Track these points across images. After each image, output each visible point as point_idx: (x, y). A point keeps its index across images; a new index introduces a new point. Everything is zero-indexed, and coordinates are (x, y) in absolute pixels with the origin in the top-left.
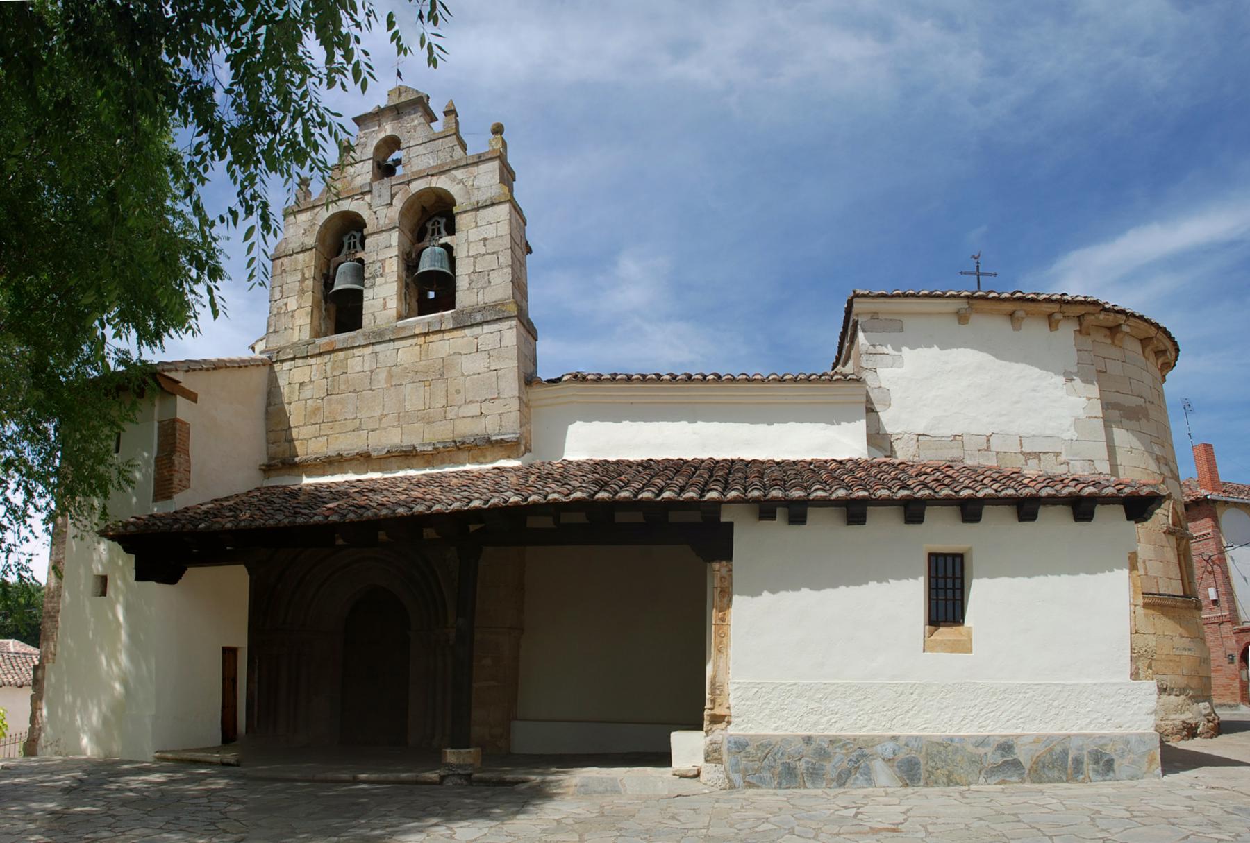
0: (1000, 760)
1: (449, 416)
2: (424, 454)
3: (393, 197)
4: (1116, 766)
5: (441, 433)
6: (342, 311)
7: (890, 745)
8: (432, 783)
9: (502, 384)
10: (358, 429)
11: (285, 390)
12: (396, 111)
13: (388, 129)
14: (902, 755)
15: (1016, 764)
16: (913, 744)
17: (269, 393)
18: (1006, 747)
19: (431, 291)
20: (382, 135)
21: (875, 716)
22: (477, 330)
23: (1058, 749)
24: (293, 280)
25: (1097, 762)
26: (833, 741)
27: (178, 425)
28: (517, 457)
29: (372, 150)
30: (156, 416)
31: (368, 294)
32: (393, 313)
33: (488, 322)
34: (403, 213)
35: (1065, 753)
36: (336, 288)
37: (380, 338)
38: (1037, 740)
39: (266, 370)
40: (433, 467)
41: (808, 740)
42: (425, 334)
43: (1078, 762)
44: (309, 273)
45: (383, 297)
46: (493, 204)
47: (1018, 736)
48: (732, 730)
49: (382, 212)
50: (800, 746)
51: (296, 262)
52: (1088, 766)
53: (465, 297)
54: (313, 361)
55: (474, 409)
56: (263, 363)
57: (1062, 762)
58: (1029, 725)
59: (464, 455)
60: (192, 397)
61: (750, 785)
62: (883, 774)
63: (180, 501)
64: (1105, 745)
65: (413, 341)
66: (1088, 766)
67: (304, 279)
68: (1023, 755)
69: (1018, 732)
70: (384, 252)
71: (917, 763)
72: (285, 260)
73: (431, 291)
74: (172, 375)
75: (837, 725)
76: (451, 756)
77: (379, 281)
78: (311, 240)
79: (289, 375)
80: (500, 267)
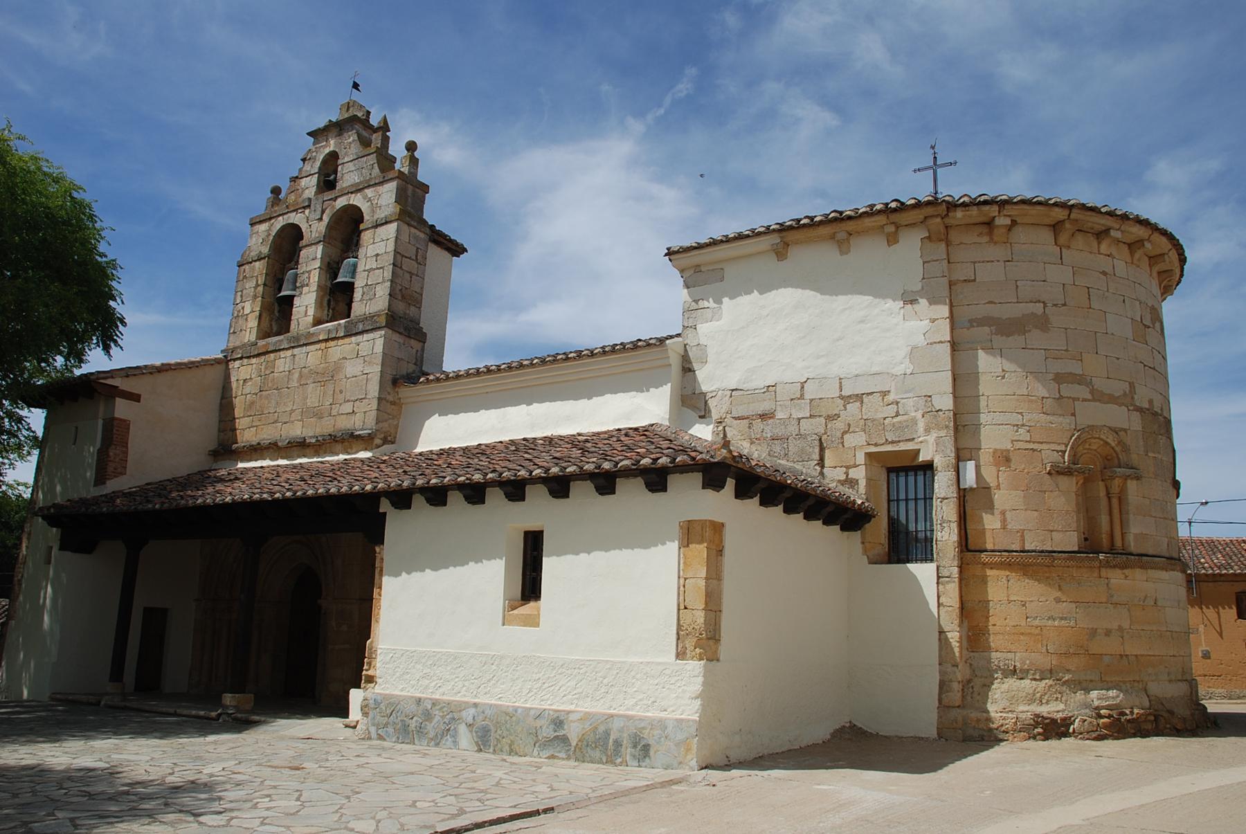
0: (553, 734)
1: (334, 412)
2: (309, 445)
3: (323, 212)
4: (652, 752)
5: (325, 427)
6: (278, 312)
7: (472, 711)
8: (212, 719)
9: (369, 386)
10: (276, 422)
11: (234, 385)
12: (337, 128)
13: (331, 145)
14: (479, 723)
15: (564, 740)
16: (488, 712)
17: (224, 387)
18: (558, 723)
19: (338, 296)
20: (327, 151)
21: (466, 684)
22: (359, 338)
23: (602, 729)
24: (250, 284)
25: (635, 747)
26: (435, 703)
27: (115, 423)
28: (370, 450)
29: (318, 164)
30: (101, 414)
31: (297, 301)
32: (310, 319)
33: (367, 331)
34: (330, 227)
35: (607, 733)
36: (282, 294)
37: (297, 343)
38: (587, 716)
39: (223, 367)
40: (319, 456)
41: (419, 701)
42: (326, 340)
43: (618, 744)
44: (261, 281)
45: (306, 304)
46: (386, 223)
47: (569, 712)
48: (378, 689)
49: (315, 225)
50: (413, 707)
51: (253, 269)
52: (628, 751)
53: (358, 309)
54: (254, 361)
55: (348, 408)
56: (217, 361)
57: (604, 743)
58: (580, 702)
59: (339, 447)
60: (136, 398)
61: (380, 738)
62: (465, 738)
63: (112, 486)
64: (644, 728)
65: (317, 346)
66: (628, 751)
67: (257, 285)
68: (573, 732)
69: (572, 707)
70: (311, 261)
71: (489, 731)
72: (247, 267)
73: (338, 296)
74: (109, 382)
75: (441, 690)
76: (228, 699)
77: (305, 289)
78: (265, 250)
79: (241, 372)
80: (384, 281)
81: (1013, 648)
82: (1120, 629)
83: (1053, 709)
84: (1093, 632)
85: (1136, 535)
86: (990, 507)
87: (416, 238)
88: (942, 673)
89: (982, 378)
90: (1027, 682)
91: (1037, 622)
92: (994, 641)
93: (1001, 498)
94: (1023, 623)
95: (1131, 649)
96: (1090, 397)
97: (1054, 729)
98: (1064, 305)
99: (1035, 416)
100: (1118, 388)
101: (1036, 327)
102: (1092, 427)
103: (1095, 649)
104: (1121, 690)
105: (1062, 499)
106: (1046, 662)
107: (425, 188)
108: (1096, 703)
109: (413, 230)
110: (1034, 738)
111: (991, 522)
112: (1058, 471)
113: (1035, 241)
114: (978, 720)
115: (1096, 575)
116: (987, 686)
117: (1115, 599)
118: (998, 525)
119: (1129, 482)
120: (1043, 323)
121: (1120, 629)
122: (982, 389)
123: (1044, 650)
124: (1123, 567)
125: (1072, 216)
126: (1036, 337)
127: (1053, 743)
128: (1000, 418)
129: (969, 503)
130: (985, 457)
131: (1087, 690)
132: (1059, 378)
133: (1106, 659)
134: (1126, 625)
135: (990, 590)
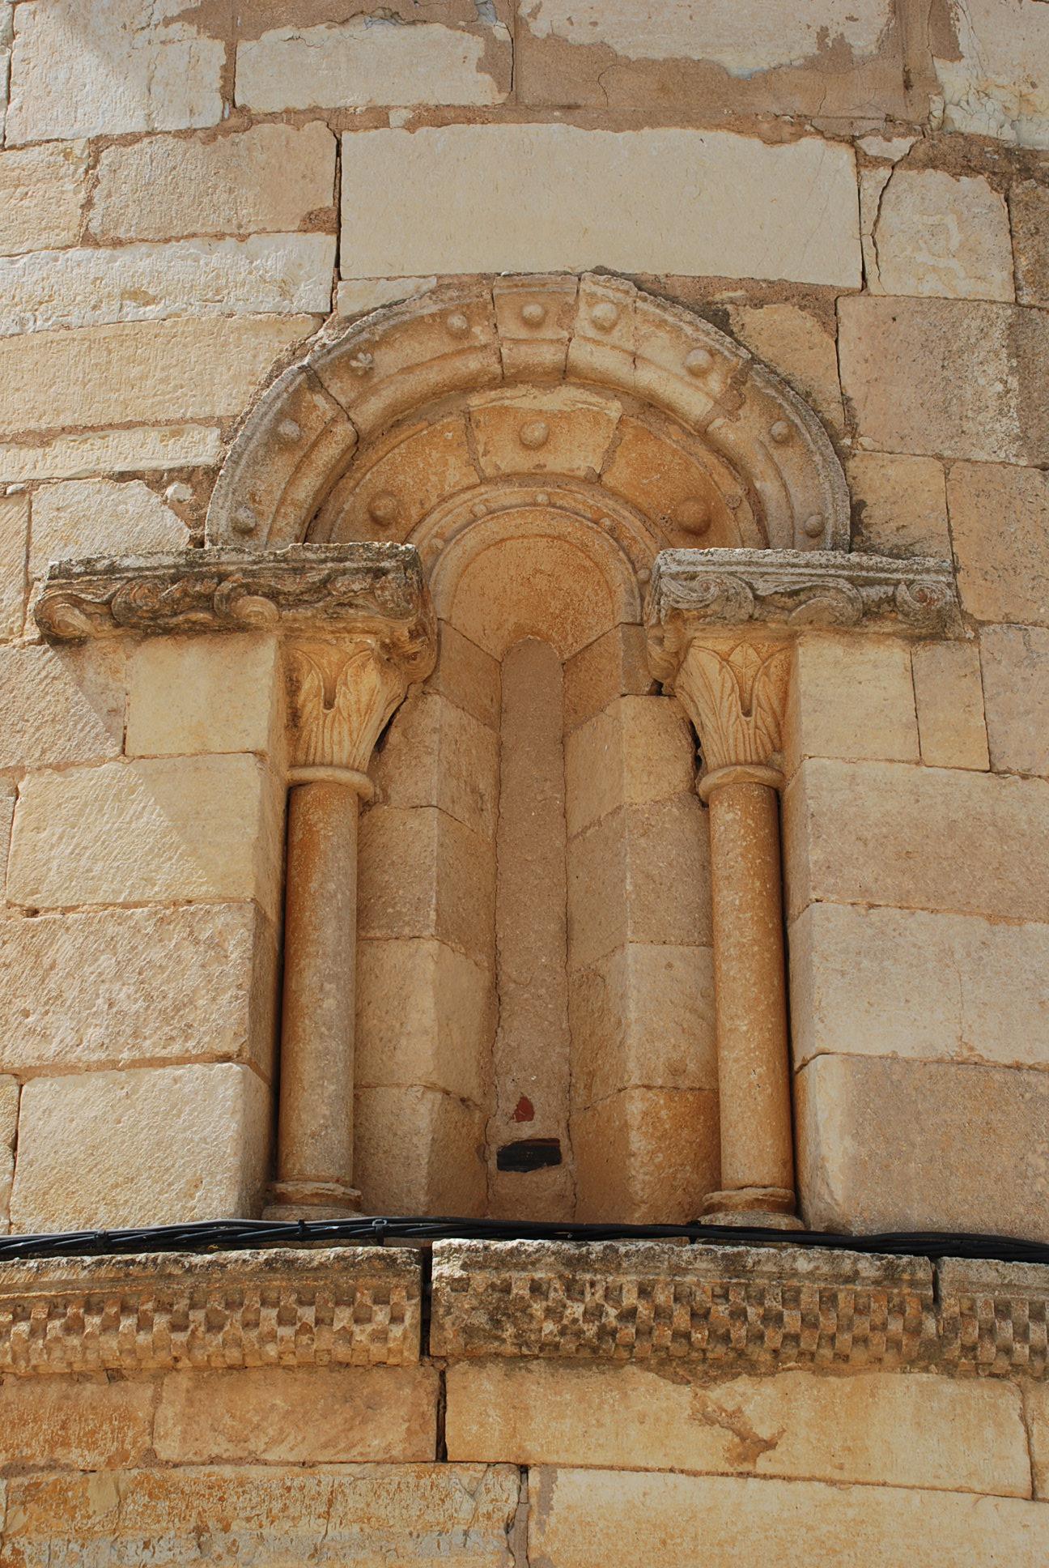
96: (482, 90)
102: (476, 297)
115: (393, 1429)
124: (703, 1351)
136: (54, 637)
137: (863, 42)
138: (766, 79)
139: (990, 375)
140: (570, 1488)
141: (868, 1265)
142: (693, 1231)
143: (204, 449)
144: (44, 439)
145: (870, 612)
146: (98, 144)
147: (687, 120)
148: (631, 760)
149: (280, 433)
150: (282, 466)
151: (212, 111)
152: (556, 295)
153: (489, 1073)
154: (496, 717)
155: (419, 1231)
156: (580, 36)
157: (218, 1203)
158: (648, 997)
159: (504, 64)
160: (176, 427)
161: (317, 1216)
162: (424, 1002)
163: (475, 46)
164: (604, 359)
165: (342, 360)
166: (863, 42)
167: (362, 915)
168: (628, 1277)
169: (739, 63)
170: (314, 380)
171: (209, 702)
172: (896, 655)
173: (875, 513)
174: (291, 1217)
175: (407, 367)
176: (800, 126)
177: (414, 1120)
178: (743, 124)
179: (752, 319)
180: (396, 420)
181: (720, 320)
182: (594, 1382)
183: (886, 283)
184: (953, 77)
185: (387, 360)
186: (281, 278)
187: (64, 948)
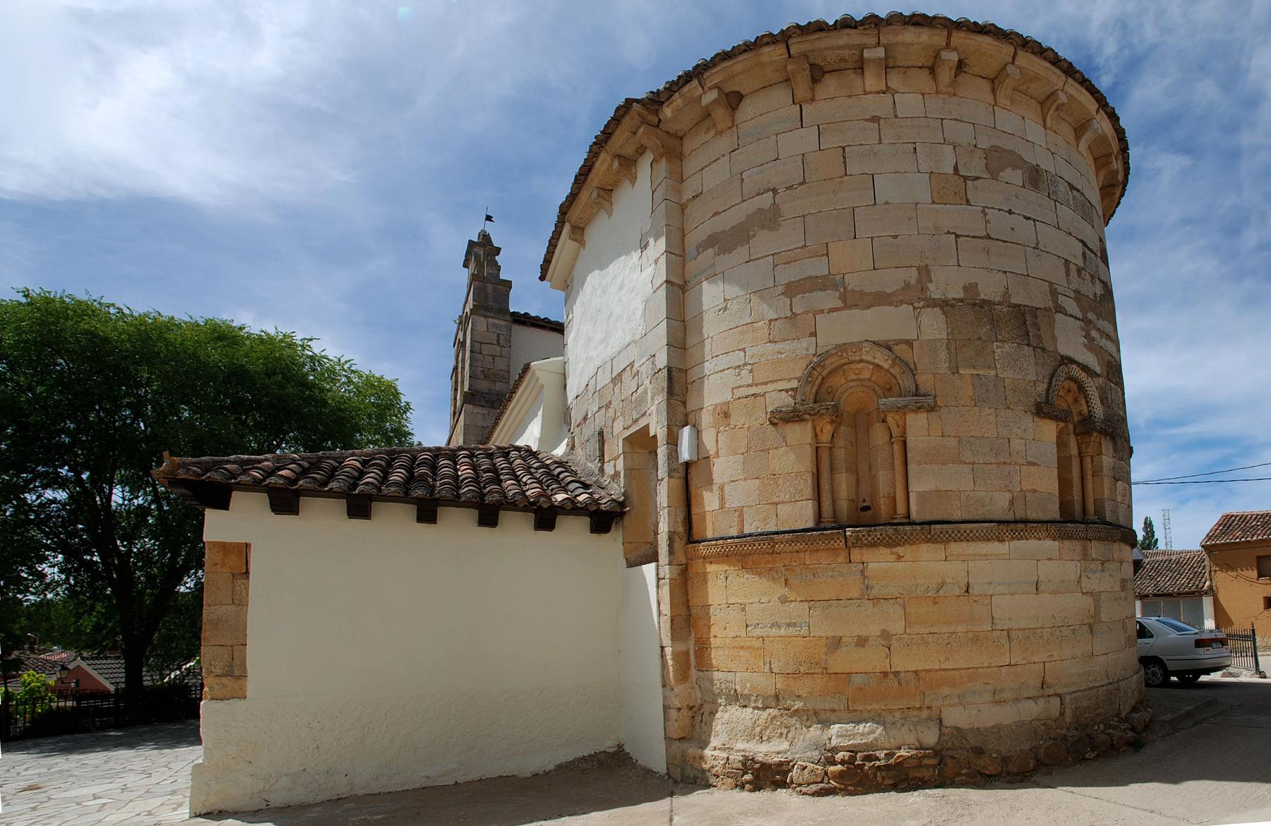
81: (733, 666)
82: (885, 635)
83: (769, 751)
84: (836, 643)
85: (921, 495)
86: (710, 482)
87: (497, 326)
88: (665, 697)
89: (706, 317)
90: (749, 710)
91: (758, 632)
92: (717, 657)
93: (722, 469)
94: (743, 634)
95: (904, 662)
96: (839, 304)
97: (767, 776)
98: (804, 182)
99: (760, 349)
100: (891, 280)
101: (763, 227)
102: (843, 348)
103: (838, 664)
104: (878, 723)
105: (791, 456)
106: (767, 684)
107: (508, 284)
108: (834, 743)
109: (490, 320)
110: (743, 787)
111: (709, 501)
112: (781, 419)
113: (767, 109)
114: (695, 758)
115: (842, 558)
116: (713, 713)
117: (875, 592)
118: (716, 505)
119: (910, 417)
120: (770, 219)
121: (885, 635)
122: (706, 333)
123: (767, 669)
124: (891, 543)
125: (794, 50)
126: (764, 242)
127: (764, 796)
128: (724, 362)
129: (689, 477)
130: (706, 419)
131: (826, 724)
132: (791, 290)
133: (857, 680)
134: (897, 627)
135: (710, 591)
136: (772, 424)
137: (913, 282)
138: (894, 293)
139: (943, 355)
140: (871, 565)
141: (918, 528)
142: (890, 524)
143: (795, 384)
144: (766, 383)
145: (919, 408)
146: (770, 321)
147: (880, 305)
148: (879, 436)
149: (808, 378)
150: (809, 387)
151: (789, 314)
152: (858, 346)
153: (857, 494)
154: (854, 426)
155: (843, 527)
156: (857, 289)
157: (810, 524)
158: (884, 481)
159: (843, 297)
160: (789, 380)
161: (828, 525)
162: (844, 483)
163: (837, 294)
164: (869, 358)
165: (818, 364)
166: (913, 282)
167: (832, 469)
168: (878, 533)
169: (889, 291)
170: (814, 368)
171: (800, 434)
172: (925, 415)
173: (921, 386)
174: (823, 525)
175: (831, 363)
176: (902, 302)
177: (844, 506)
178: (890, 304)
179: (896, 348)
180: (830, 373)
181: (889, 349)
182: (874, 549)
183: (923, 337)
184: (931, 286)
185: (827, 362)
186: (802, 349)
187: (781, 481)
